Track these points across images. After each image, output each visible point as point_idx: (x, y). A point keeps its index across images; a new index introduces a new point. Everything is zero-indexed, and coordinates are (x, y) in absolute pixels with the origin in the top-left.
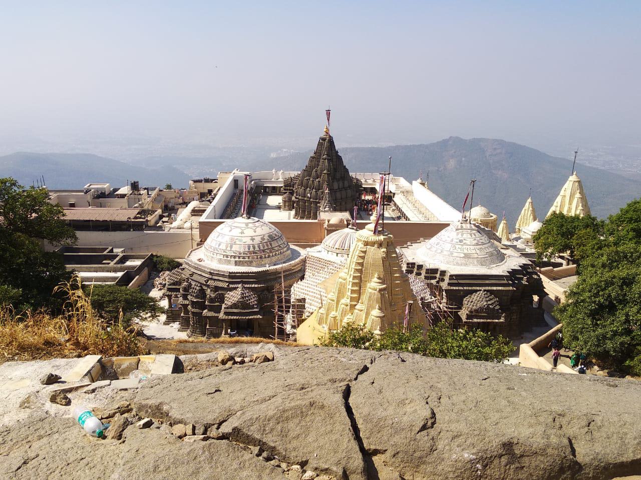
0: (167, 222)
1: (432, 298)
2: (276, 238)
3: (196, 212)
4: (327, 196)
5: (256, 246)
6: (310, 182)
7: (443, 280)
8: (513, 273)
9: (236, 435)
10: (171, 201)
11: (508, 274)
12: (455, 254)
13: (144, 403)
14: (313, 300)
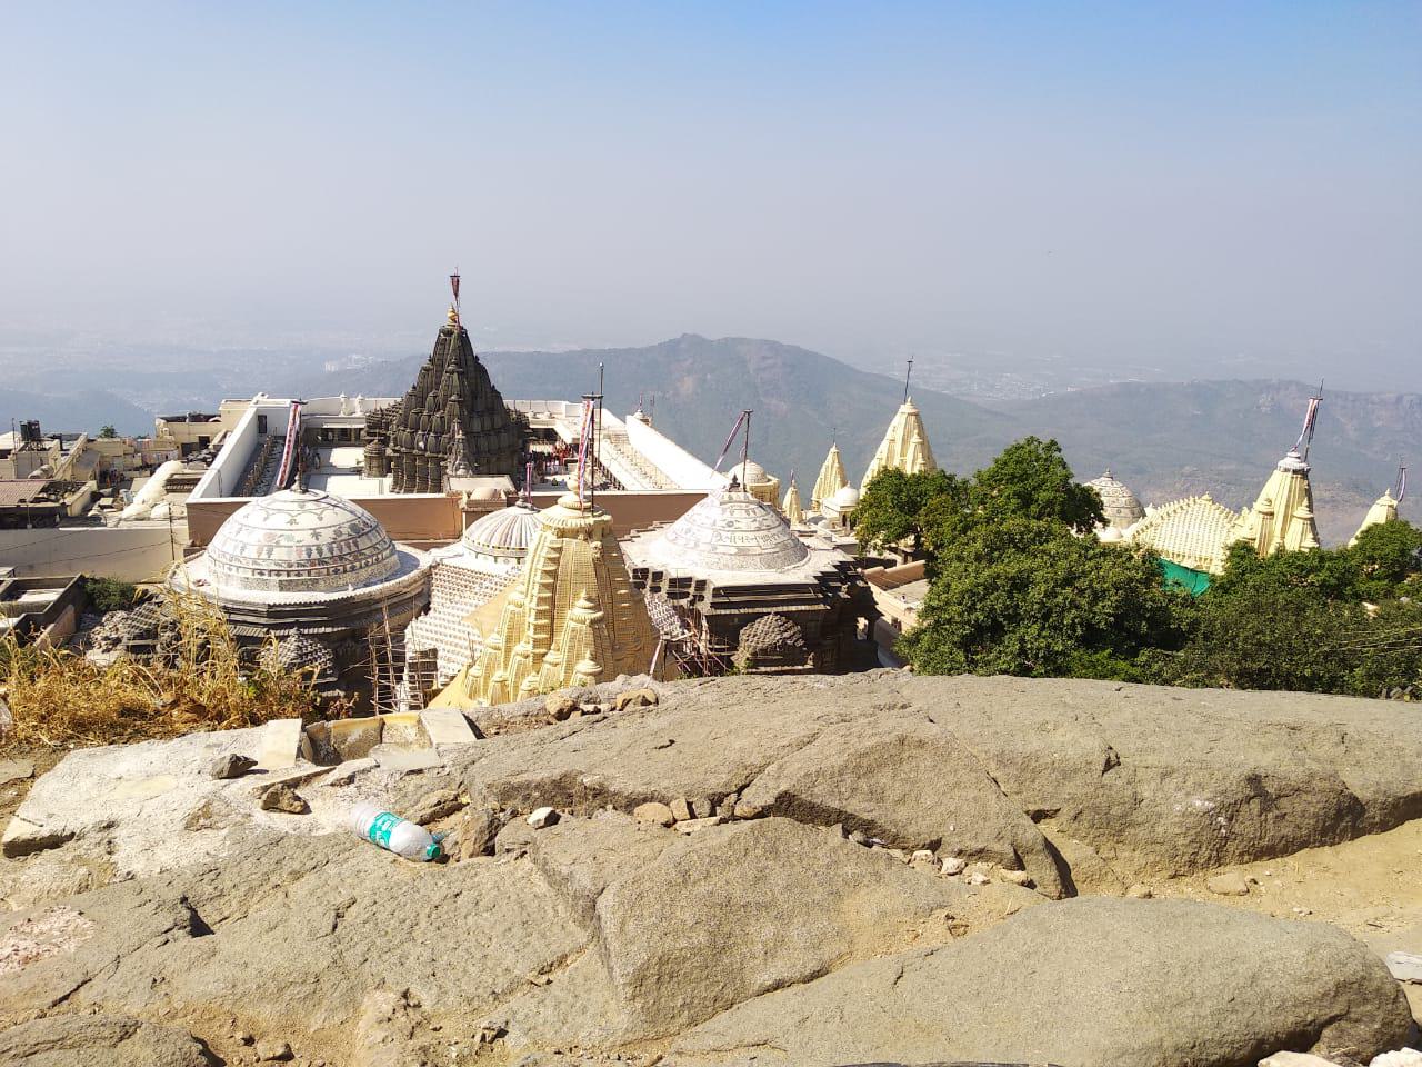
0: (112, 507)
1: (683, 633)
2: (367, 529)
3: (176, 485)
4: (461, 446)
5: (325, 548)
6: (424, 418)
7: (701, 598)
8: (824, 578)
9: (786, 805)
10: (116, 462)
11: (816, 582)
12: (721, 549)
13: (515, 780)
14: (453, 652)
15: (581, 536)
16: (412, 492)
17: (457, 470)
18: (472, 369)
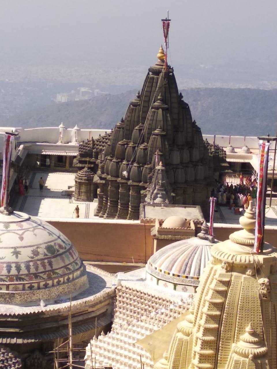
2: (61, 251)
4: (160, 176)
5: (23, 266)
6: (129, 150)
15: (249, 272)
16: (125, 218)
17: (155, 198)
18: (175, 105)
